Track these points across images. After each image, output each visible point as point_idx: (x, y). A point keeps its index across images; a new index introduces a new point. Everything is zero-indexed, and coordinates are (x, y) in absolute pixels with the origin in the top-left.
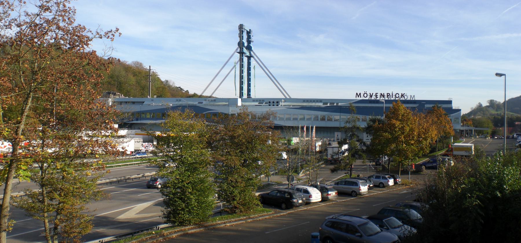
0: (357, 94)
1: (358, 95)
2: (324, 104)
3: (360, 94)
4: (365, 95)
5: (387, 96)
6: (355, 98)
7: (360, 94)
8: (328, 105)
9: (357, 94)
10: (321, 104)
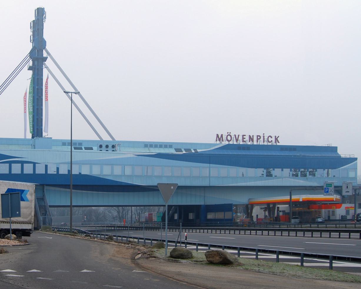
0: (218, 135)
1: (219, 138)
2: (177, 150)
3: (222, 135)
4: (229, 138)
5: (258, 139)
7: (222, 135)
8: (184, 152)
9: (218, 135)
10: (172, 151)
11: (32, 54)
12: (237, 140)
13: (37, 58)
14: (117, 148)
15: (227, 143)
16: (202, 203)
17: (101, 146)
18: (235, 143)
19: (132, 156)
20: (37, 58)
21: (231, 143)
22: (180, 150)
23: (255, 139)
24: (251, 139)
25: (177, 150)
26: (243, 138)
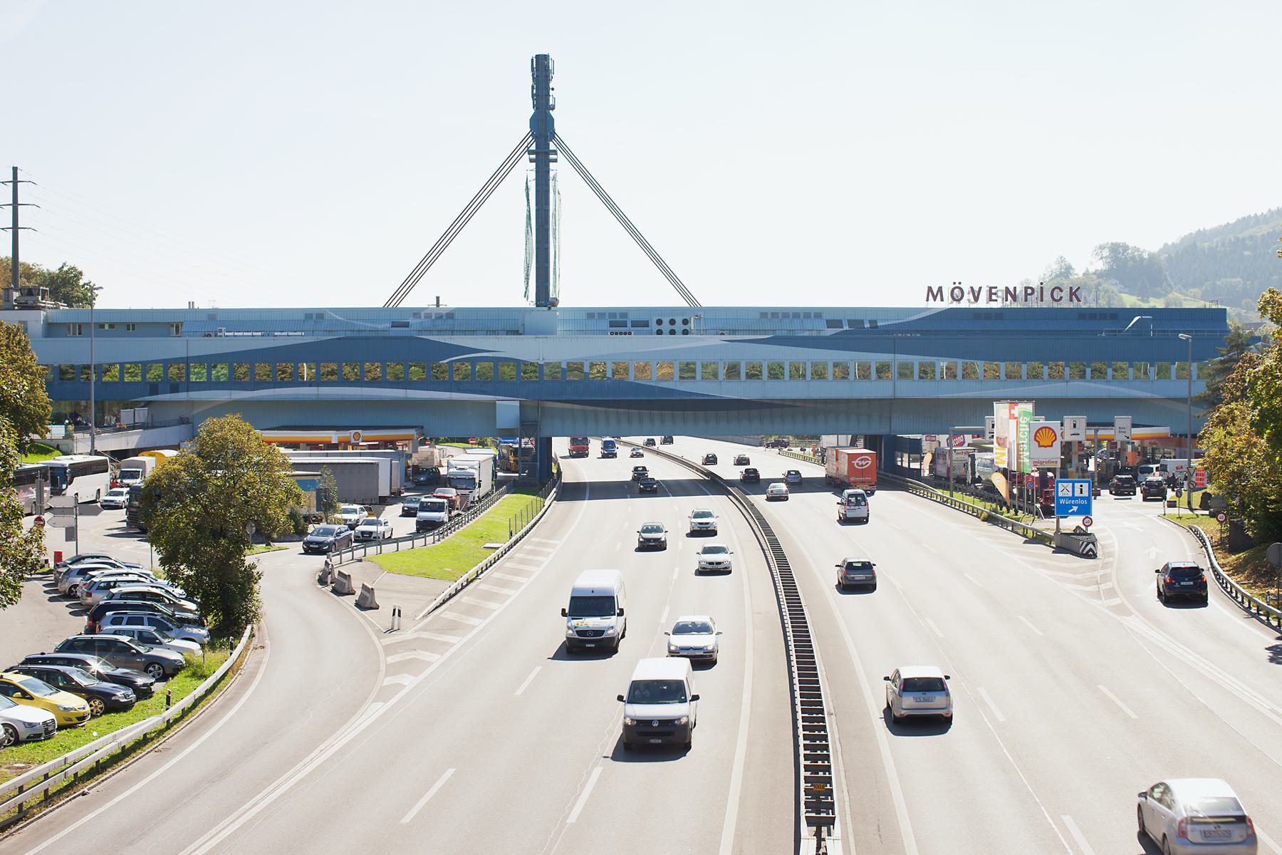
0: (930, 289)
1: (933, 293)
3: (940, 289)
6: (921, 303)
7: (940, 289)
8: (846, 328)
9: (930, 289)
11: (533, 121)
26: (991, 294)
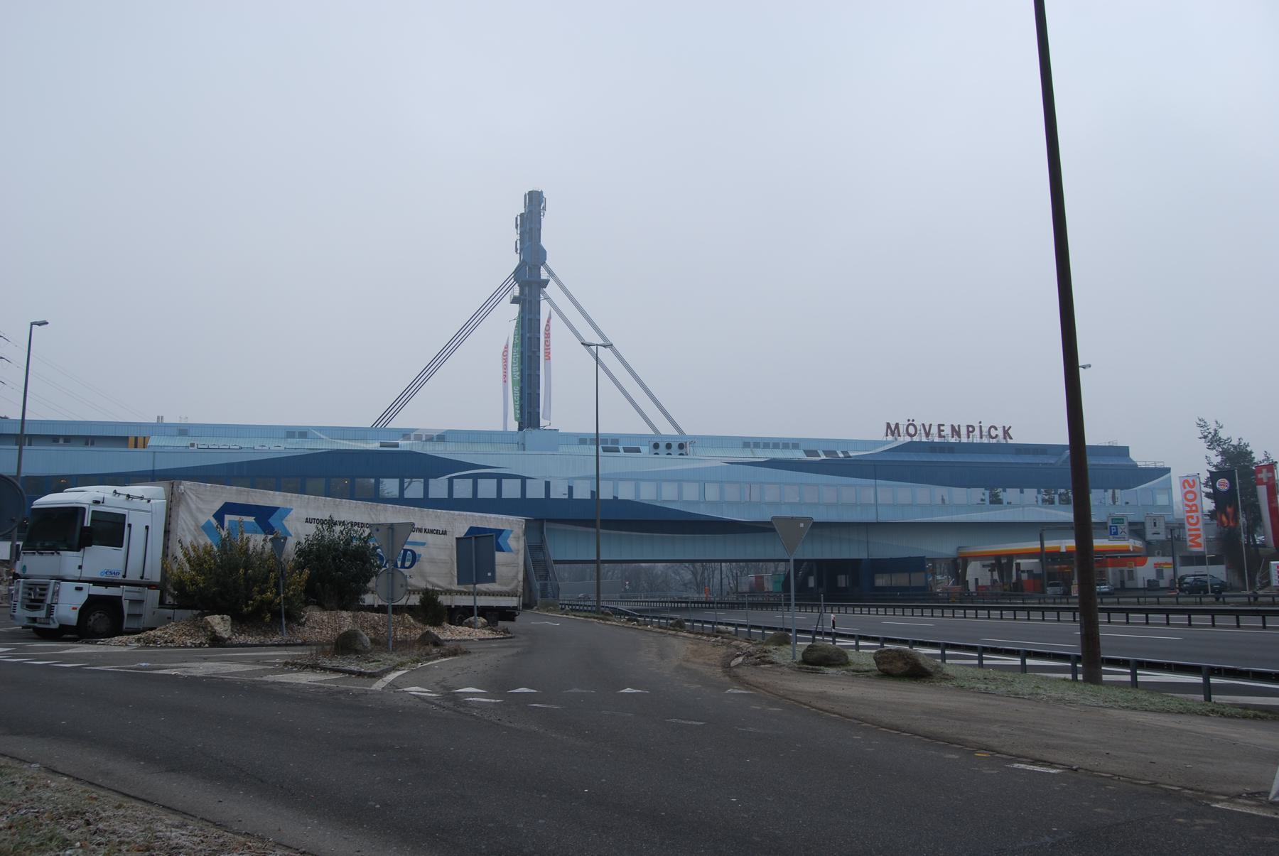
0: (888, 425)
1: (892, 430)
2: (808, 453)
3: (897, 425)
5: (969, 432)
7: (897, 425)
8: (823, 457)
9: (888, 425)
10: (799, 455)
12: (927, 434)
13: (530, 281)
14: (689, 449)
15: (908, 439)
16: (863, 556)
17: (656, 446)
18: (924, 439)
19: (719, 464)
20: (530, 281)
21: (916, 439)
22: (815, 453)
23: (964, 431)
24: (955, 431)
25: (808, 453)
26: (940, 431)
